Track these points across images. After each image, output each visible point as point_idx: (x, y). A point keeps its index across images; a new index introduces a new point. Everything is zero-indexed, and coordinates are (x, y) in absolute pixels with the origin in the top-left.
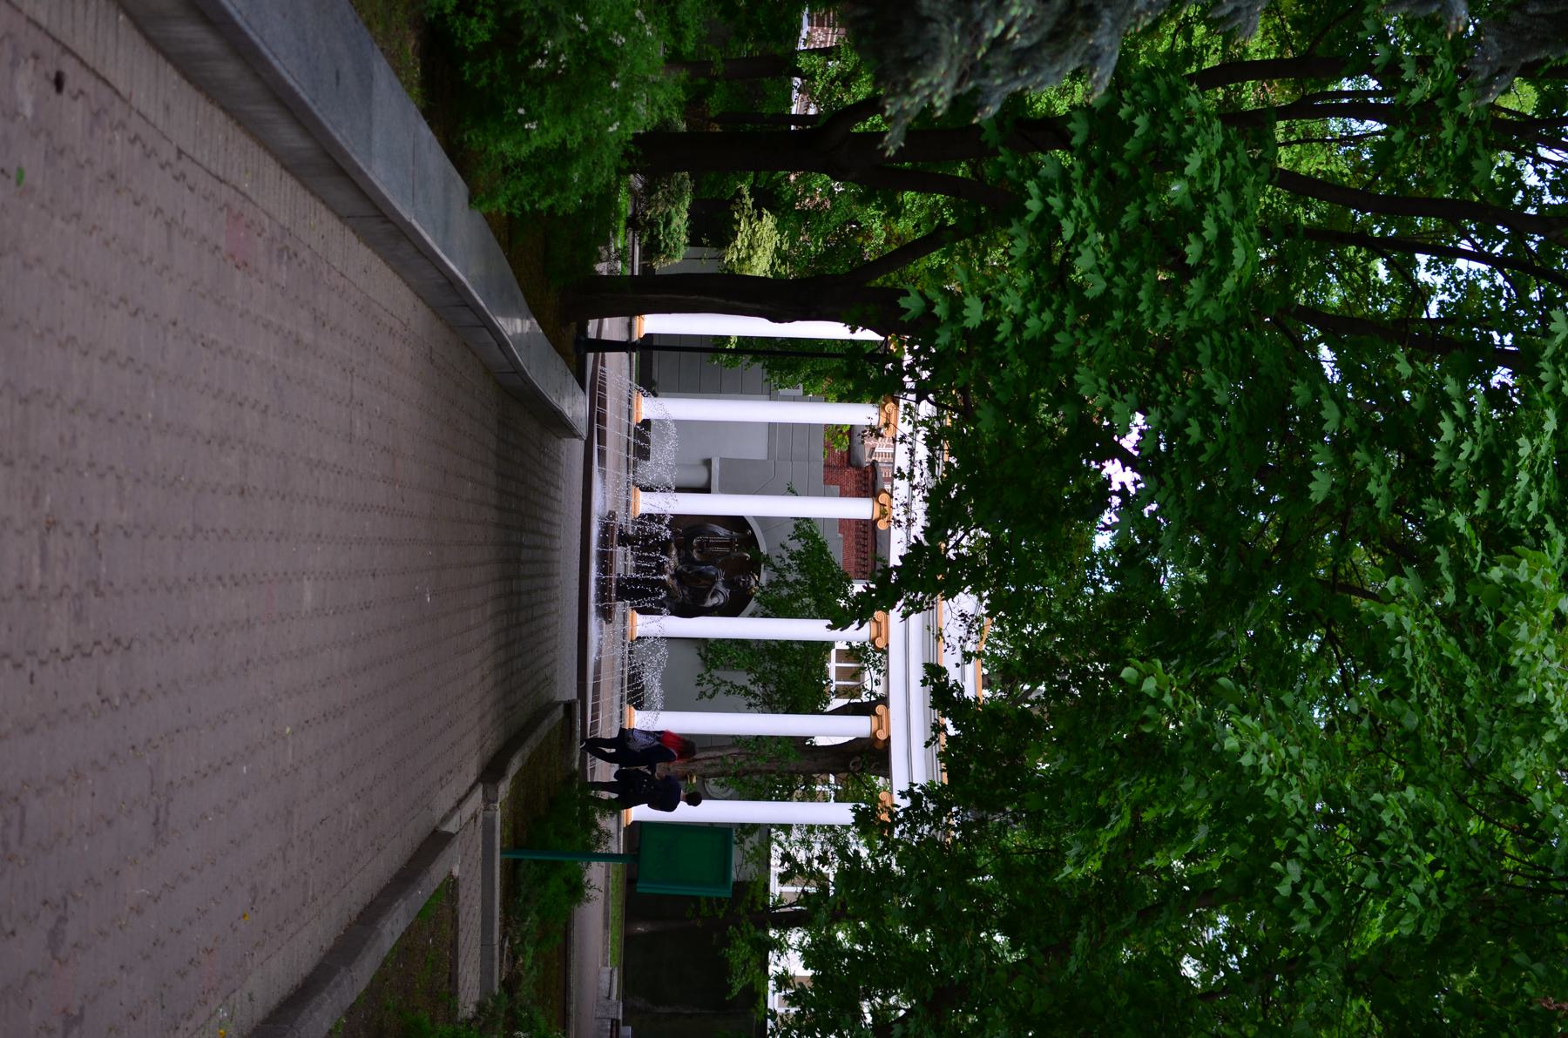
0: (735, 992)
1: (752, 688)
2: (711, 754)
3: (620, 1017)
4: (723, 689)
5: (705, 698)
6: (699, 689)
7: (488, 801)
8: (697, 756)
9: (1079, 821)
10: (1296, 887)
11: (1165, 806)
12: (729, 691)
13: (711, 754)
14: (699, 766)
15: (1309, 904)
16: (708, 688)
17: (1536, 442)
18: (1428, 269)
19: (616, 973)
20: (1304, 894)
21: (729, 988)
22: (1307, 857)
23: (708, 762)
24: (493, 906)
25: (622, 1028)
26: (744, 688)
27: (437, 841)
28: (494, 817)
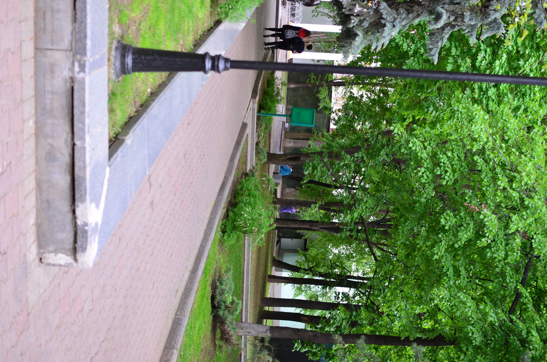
0: (321, 108)
1: (330, 14)
2: (316, 35)
3: (285, 121)
4: (320, 14)
5: (314, 17)
6: (313, 14)
7: (254, 103)
8: (311, 36)
9: (399, 121)
10: (423, 173)
11: (421, 116)
12: (322, 15)
13: (316, 35)
14: (311, 39)
15: (425, 177)
16: (316, 14)
17: (500, 61)
18: (424, 105)
19: (284, 107)
20: (424, 175)
21: (319, 106)
22: (426, 167)
23: (314, 38)
24: (254, 129)
25: (285, 124)
26: (327, 14)
27: (244, 126)
28: (255, 107)
